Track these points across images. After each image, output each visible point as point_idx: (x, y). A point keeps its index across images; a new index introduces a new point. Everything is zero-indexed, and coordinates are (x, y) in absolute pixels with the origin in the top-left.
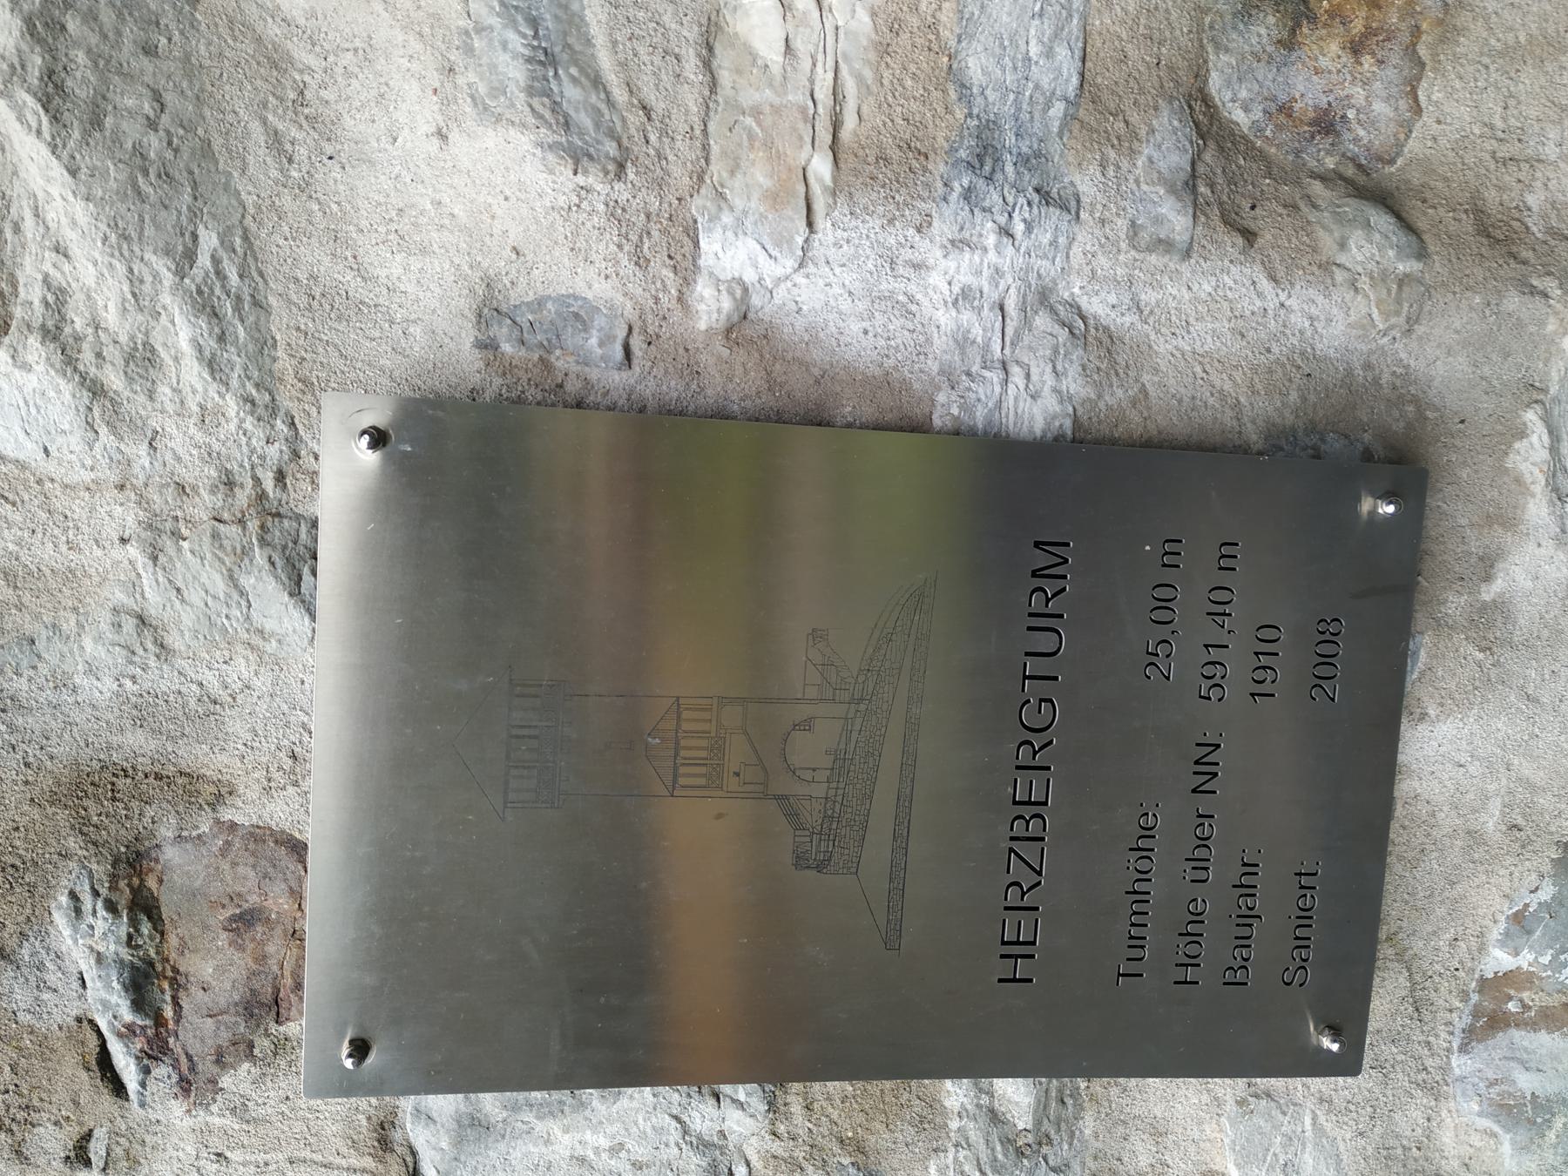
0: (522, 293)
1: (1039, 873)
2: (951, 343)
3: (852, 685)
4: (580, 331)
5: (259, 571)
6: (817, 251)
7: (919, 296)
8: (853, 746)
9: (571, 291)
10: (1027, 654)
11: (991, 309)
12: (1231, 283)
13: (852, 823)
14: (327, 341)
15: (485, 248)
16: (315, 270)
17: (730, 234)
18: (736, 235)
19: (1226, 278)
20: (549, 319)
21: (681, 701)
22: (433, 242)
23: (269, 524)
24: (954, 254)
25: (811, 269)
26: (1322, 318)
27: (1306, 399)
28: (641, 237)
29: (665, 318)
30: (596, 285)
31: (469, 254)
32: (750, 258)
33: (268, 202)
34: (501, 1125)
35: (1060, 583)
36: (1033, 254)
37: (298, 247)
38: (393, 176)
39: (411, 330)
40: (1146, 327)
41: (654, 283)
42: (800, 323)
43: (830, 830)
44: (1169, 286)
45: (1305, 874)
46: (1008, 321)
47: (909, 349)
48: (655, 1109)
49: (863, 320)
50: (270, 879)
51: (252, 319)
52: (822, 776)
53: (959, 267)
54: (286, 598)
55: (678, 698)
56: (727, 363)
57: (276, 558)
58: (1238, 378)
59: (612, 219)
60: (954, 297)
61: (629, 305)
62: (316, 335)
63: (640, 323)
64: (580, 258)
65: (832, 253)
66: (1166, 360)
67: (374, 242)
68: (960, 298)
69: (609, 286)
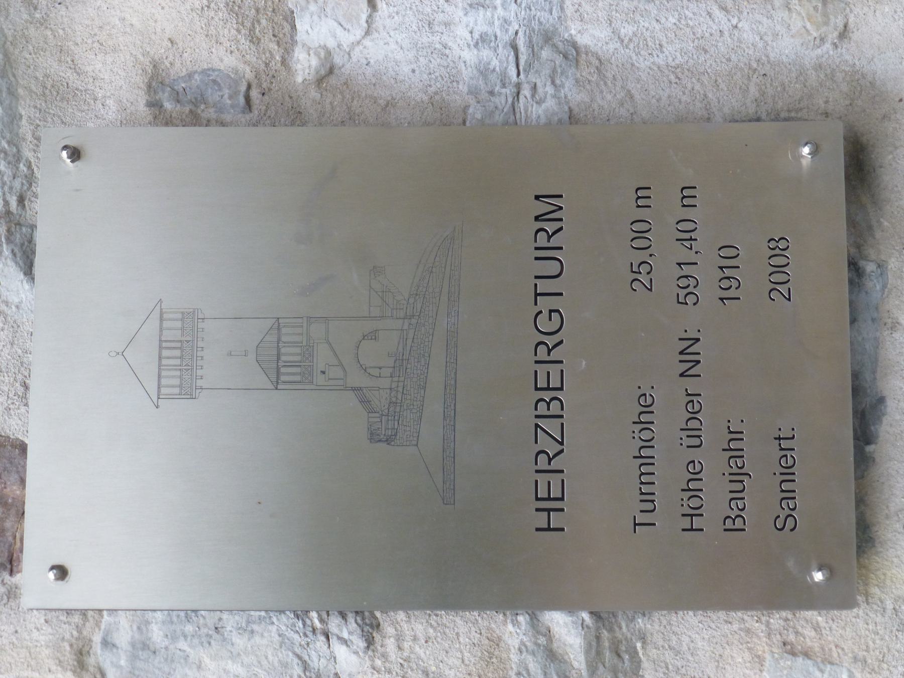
0: (179, 69)
1: (562, 443)
2: (475, 72)
3: (405, 306)
4: (216, 91)
5: (6, 259)
6: (378, 22)
7: (450, 44)
8: (408, 348)
9: (210, 66)
10: (536, 277)
11: (504, 47)
12: (691, 15)
13: (412, 407)
14: (54, 114)
15: (151, 42)
16: (48, 71)
17: (315, 17)
18: (320, 18)
19: (687, 12)
20: (196, 85)
21: (281, 321)
22: (120, 44)
23: (13, 230)
24: (472, 13)
25: (375, 35)
26: (769, 34)
27: (764, 93)
28: (253, 24)
29: (274, 77)
30: (226, 59)
31: (141, 47)
32: (330, 32)
33: (20, 33)
34: (163, 650)
35: (557, 225)
36: (533, 8)
37: (38, 58)
38: (96, 8)
39: (108, 102)
40: (627, 51)
41: (264, 53)
42: (369, 71)
43: (395, 412)
44: (641, 21)
45: (783, 439)
46: (520, 56)
47: (445, 79)
48: (281, 647)
49: (411, 63)
50: (8, 471)
51: (7, 102)
52: (387, 372)
53: (476, 21)
54: (22, 276)
55: (278, 318)
56: (319, 103)
57: (16, 250)
58: (705, 81)
59: (231, 13)
60: (475, 41)
61: (248, 69)
62: (47, 110)
63: (256, 81)
64: (213, 41)
65: (388, 22)
66: (646, 72)
67: (84, 50)
68: (479, 41)
69: (233, 59)
